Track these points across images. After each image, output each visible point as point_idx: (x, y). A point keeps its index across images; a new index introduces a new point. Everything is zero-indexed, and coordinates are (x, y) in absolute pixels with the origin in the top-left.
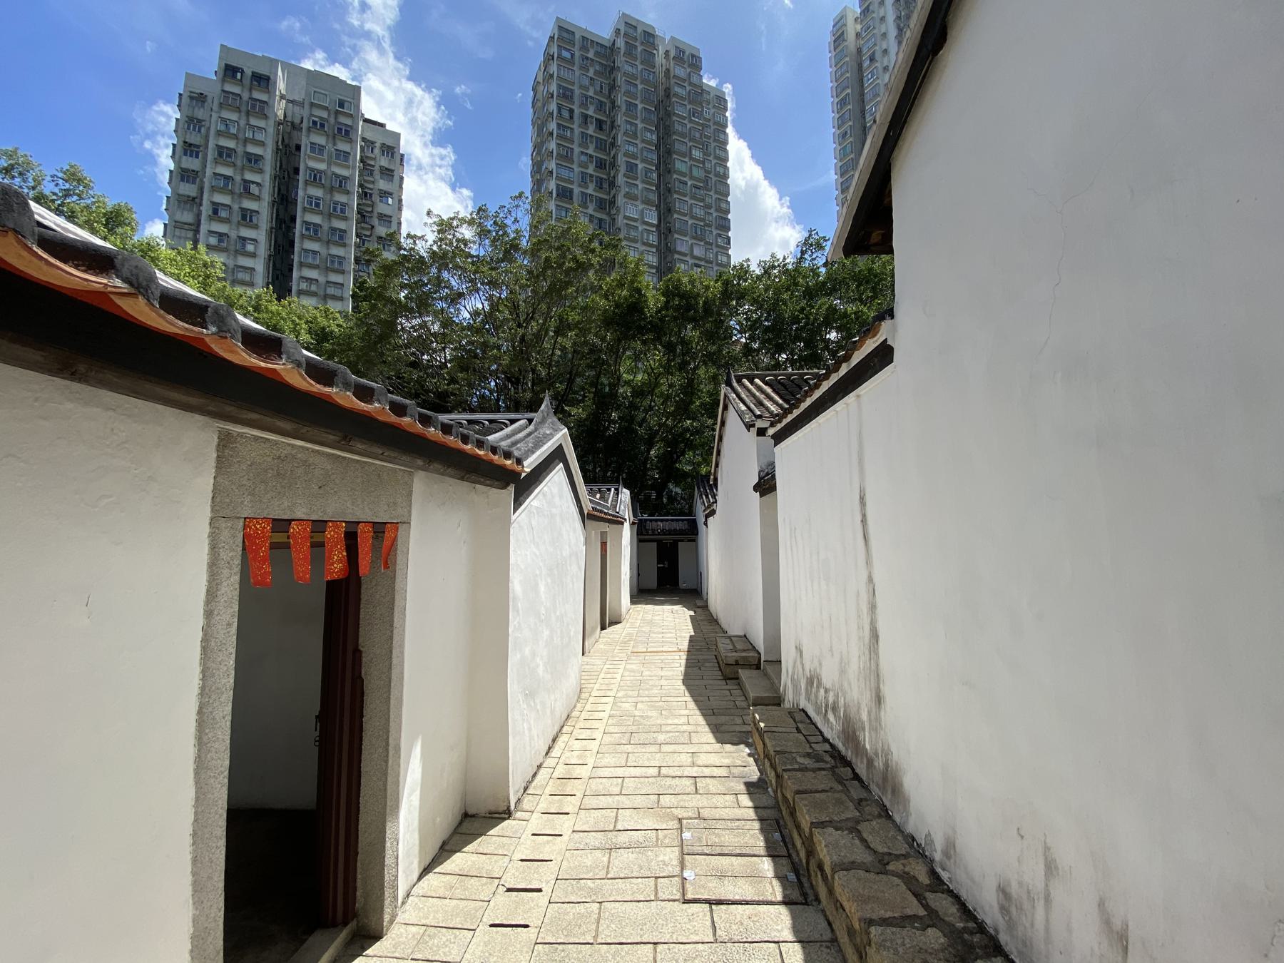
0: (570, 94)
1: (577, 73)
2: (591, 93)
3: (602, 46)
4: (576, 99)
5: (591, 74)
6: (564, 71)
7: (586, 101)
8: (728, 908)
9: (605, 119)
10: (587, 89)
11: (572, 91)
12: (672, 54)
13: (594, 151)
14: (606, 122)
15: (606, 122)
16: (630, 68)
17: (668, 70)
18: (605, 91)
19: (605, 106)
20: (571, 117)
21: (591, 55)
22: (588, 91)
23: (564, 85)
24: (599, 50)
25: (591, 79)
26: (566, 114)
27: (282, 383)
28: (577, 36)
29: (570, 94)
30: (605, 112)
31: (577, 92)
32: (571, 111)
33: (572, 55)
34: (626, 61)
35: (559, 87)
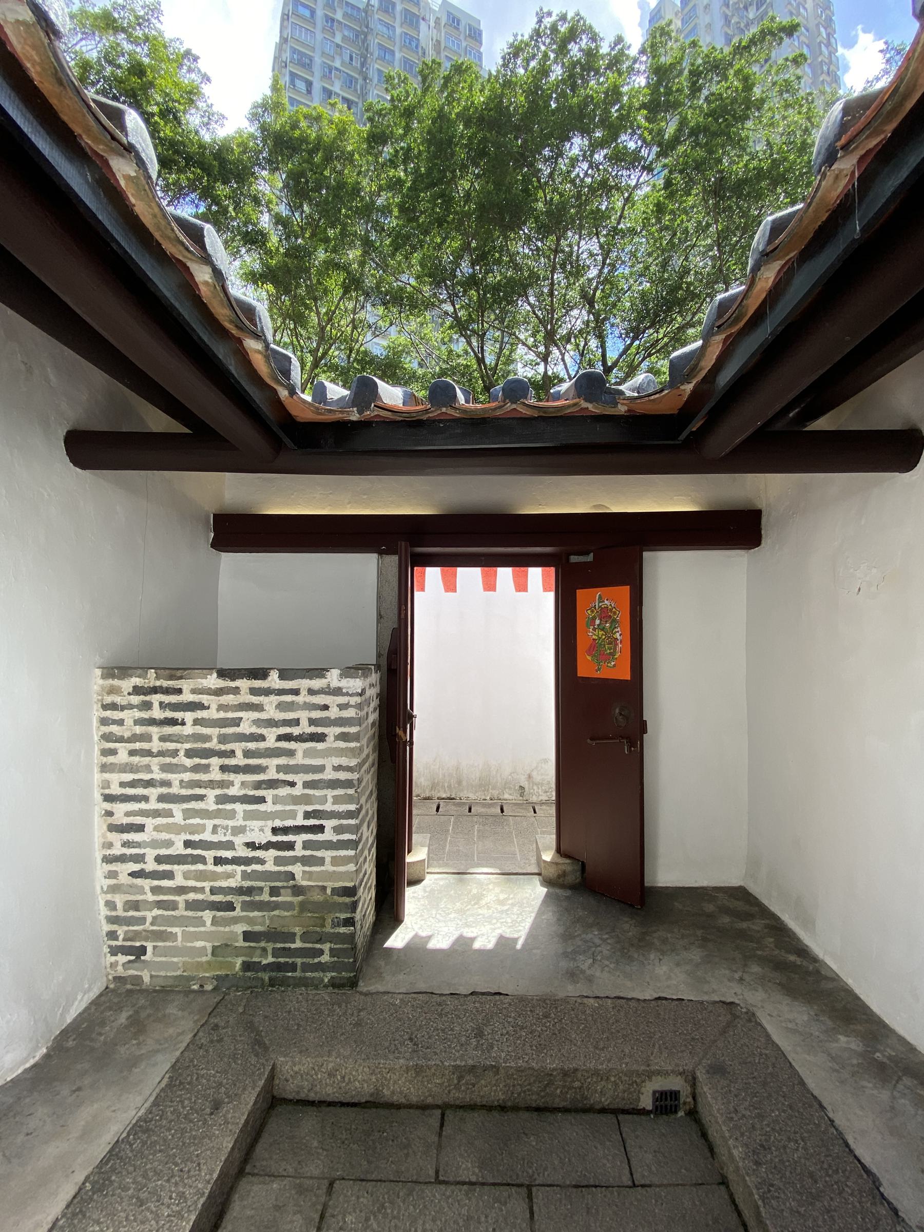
0: (307, 61)
1: (319, 36)
2: (337, 64)
3: (353, 7)
4: (317, 69)
5: (338, 39)
6: (301, 31)
7: (330, 72)
8: (410, 915)
9: (356, 100)
10: (333, 59)
11: (311, 59)
12: (444, 21)
13: (341, 90)
14: (357, 103)
15: (357, 103)
16: (385, 29)
17: (438, 42)
18: (357, 63)
19: (356, 83)
20: (309, 92)
21: (339, 16)
22: (333, 61)
23: (301, 49)
24: (349, 11)
25: (338, 46)
26: (301, 85)
27: (115, 188)
28: (463, 23)
29: (307, 61)
30: (356, 90)
31: (318, 60)
32: (309, 84)
33: (313, 12)
34: (380, 20)
35: (294, 51)
